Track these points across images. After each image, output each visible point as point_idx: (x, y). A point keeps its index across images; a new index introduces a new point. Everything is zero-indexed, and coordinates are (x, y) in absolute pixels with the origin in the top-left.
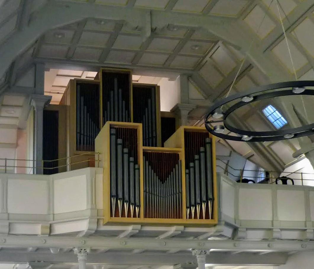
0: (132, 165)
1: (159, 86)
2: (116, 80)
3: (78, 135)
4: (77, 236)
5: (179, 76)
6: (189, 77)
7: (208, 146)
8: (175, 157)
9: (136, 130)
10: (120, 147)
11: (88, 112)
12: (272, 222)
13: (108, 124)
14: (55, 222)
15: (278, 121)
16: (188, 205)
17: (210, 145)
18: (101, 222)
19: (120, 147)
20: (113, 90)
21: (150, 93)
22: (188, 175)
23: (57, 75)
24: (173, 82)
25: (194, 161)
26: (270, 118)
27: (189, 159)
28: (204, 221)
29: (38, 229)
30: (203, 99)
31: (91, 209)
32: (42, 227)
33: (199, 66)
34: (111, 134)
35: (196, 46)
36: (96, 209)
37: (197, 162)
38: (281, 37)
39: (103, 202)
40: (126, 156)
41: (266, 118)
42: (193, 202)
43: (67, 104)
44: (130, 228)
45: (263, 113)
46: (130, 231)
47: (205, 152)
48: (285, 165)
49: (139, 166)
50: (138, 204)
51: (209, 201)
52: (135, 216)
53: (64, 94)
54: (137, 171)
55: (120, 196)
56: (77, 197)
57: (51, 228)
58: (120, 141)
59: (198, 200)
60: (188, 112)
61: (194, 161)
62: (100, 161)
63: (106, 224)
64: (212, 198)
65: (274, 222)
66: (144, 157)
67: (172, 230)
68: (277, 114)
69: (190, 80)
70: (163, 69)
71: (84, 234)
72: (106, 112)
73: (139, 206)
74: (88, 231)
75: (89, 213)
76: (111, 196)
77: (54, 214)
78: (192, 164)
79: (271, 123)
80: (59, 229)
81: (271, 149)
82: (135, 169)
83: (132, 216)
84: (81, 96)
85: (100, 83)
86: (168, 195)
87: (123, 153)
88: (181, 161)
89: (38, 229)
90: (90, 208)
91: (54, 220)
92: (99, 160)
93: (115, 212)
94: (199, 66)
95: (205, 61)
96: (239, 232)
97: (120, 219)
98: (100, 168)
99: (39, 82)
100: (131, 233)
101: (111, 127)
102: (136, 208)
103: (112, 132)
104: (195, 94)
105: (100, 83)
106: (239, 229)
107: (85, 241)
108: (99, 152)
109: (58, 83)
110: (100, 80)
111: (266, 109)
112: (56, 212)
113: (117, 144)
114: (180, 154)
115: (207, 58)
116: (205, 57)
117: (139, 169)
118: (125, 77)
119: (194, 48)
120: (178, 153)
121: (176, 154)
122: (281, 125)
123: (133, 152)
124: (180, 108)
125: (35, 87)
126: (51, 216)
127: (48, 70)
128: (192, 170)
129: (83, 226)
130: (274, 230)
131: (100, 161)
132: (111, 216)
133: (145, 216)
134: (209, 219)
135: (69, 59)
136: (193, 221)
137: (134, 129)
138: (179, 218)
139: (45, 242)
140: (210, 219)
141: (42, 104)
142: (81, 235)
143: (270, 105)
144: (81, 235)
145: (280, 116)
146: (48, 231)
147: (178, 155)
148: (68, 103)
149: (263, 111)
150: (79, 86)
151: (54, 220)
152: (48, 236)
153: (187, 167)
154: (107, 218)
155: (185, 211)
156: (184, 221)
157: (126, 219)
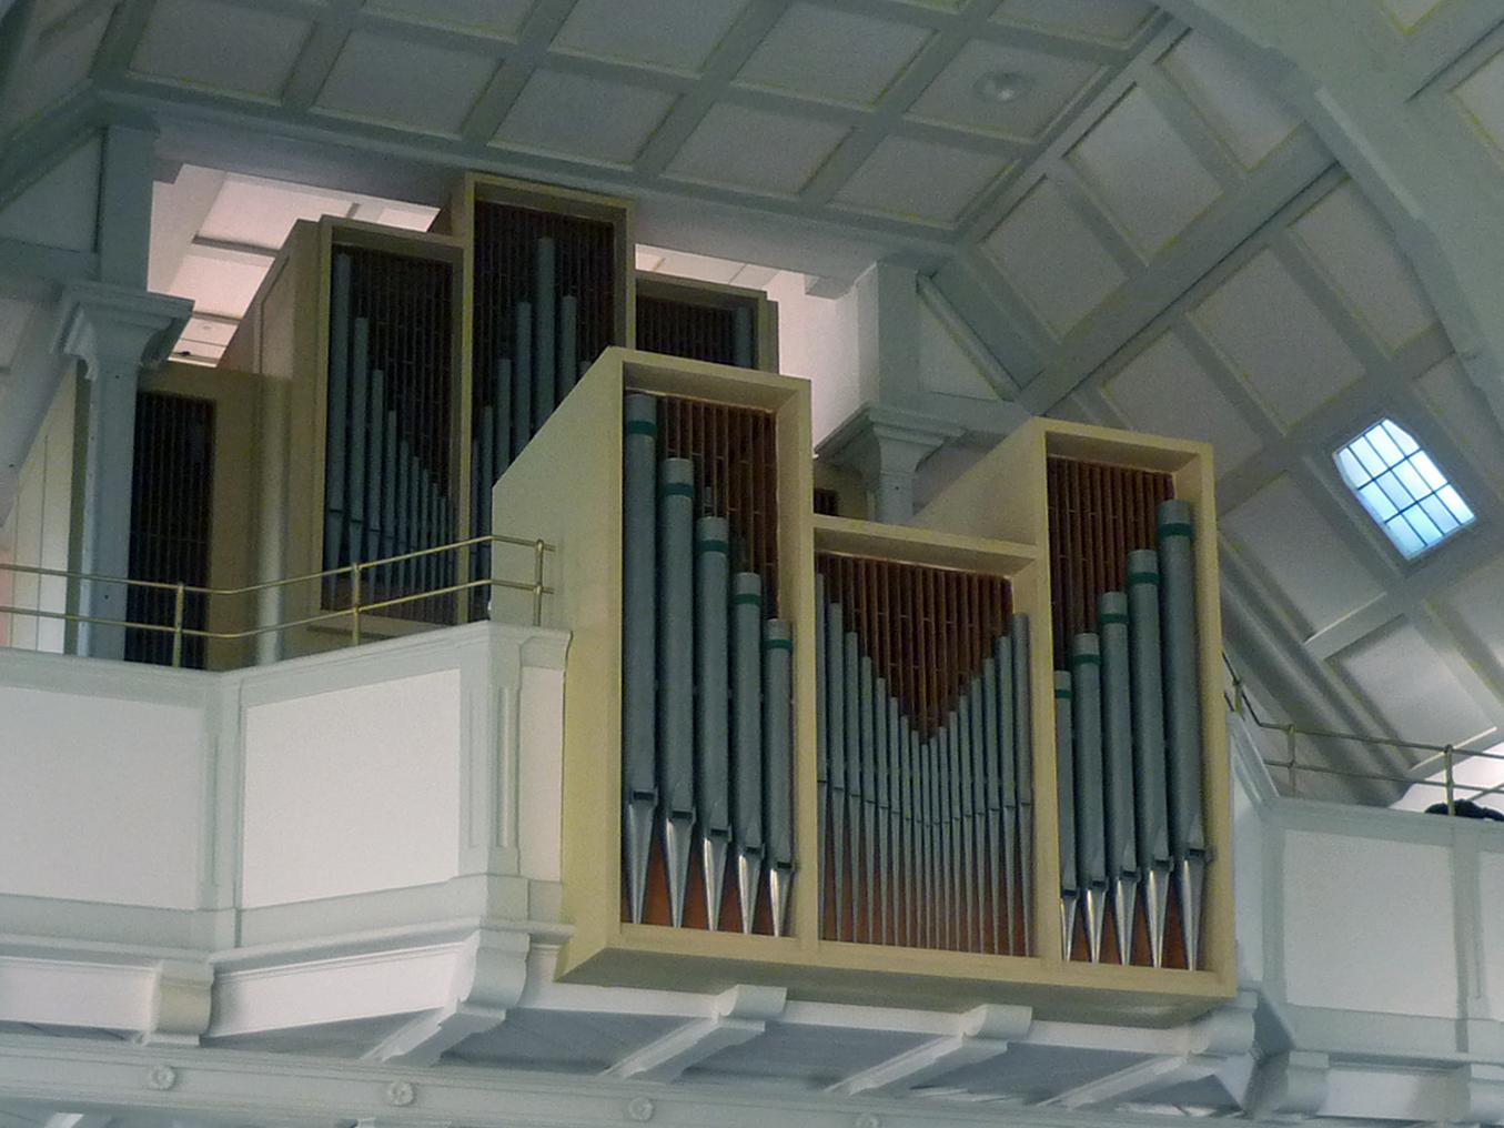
0: (748, 615)
1: (776, 303)
2: (546, 249)
3: (336, 523)
4: (369, 1054)
5: (874, 265)
6: (926, 272)
7: (1174, 545)
8: (983, 597)
9: (769, 422)
10: (679, 506)
11: (389, 404)
12: (1461, 1024)
13: (609, 367)
14: (243, 953)
15: (1415, 515)
16: (1071, 884)
17: (1183, 539)
18: (549, 963)
19: (679, 506)
20: (533, 300)
21: (726, 326)
22: (1067, 703)
23: (198, 240)
24: (830, 301)
25: (1097, 624)
26: (1373, 498)
27: (1074, 613)
28: (1155, 980)
29: (137, 998)
30: (995, 397)
31: (489, 874)
32: (165, 983)
33: (986, 212)
34: (629, 428)
35: (1006, 79)
36: (518, 876)
37: (1116, 632)
38: (1456, 67)
39: (570, 829)
40: (715, 563)
41: (1351, 496)
42: (1096, 868)
43: (267, 372)
44: (715, 1009)
45: (1335, 473)
46: (714, 1024)
47: (1161, 580)
48: (1413, 765)
49: (791, 627)
50: (785, 859)
51: (1152, 874)
52: (762, 926)
53: (228, 347)
54: (777, 657)
55: (681, 797)
56: (400, 797)
57: (218, 987)
58: (680, 470)
59: (1126, 857)
60: (917, 456)
61: (1097, 624)
62: (550, 591)
63: (577, 970)
64: (1199, 845)
65: (1472, 1026)
66: (821, 576)
67: (957, 1032)
68: (1424, 473)
69: (926, 291)
70: (805, 217)
71: (431, 1028)
72: (489, 412)
73: (789, 868)
74: (468, 1012)
75: (475, 899)
76: (629, 795)
77: (239, 912)
78: (1086, 644)
79: (1374, 523)
80: (271, 1002)
81: (1346, 678)
82: (765, 646)
83: (747, 926)
84: (354, 312)
85: (460, 252)
86: (956, 810)
87: (698, 548)
88: (1026, 620)
89: (137, 998)
90: (485, 870)
91: (238, 945)
92: (540, 583)
93: (647, 890)
94: (986, 212)
95: (1032, 176)
96: (1288, 1072)
97: (672, 939)
98: (550, 627)
99: (116, 238)
100: (718, 1034)
101: (632, 380)
102: (773, 875)
103: (636, 416)
104: (952, 368)
105: (460, 252)
106: (1294, 1058)
107: (414, 1086)
108: (540, 541)
109: (222, 256)
110: (464, 238)
111: (1359, 445)
112: (248, 902)
113: (661, 492)
114: (1012, 582)
115: (1050, 162)
116: (1038, 152)
117: (789, 646)
118: (592, 244)
119: (990, 87)
120: (1006, 577)
121: (992, 581)
122: (1433, 536)
123: (755, 546)
124: (878, 431)
125: (96, 247)
126: (224, 925)
127: (170, 176)
128: (1088, 673)
129: (435, 984)
130: (1476, 1071)
131: (550, 591)
132: (626, 917)
133: (827, 932)
134: (1186, 967)
135: (280, 121)
136: (1094, 976)
137: (756, 416)
138: (1020, 951)
139: (175, 1082)
140: (1191, 968)
141: (133, 345)
142: (396, 1046)
143: (1387, 423)
144: (396, 1046)
145: (1436, 478)
146: (200, 1010)
147: (1005, 586)
148: (278, 362)
149: (1334, 456)
150: (345, 263)
151: (238, 945)
152: (195, 1041)
153: (1065, 658)
154: (597, 924)
155: (1052, 914)
156: (1050, 966)
157: (710, 943)
